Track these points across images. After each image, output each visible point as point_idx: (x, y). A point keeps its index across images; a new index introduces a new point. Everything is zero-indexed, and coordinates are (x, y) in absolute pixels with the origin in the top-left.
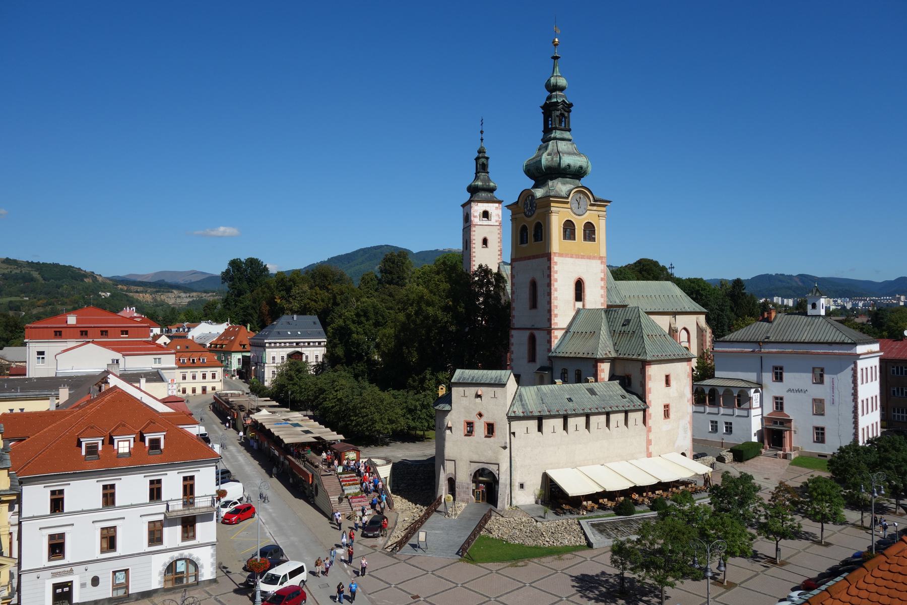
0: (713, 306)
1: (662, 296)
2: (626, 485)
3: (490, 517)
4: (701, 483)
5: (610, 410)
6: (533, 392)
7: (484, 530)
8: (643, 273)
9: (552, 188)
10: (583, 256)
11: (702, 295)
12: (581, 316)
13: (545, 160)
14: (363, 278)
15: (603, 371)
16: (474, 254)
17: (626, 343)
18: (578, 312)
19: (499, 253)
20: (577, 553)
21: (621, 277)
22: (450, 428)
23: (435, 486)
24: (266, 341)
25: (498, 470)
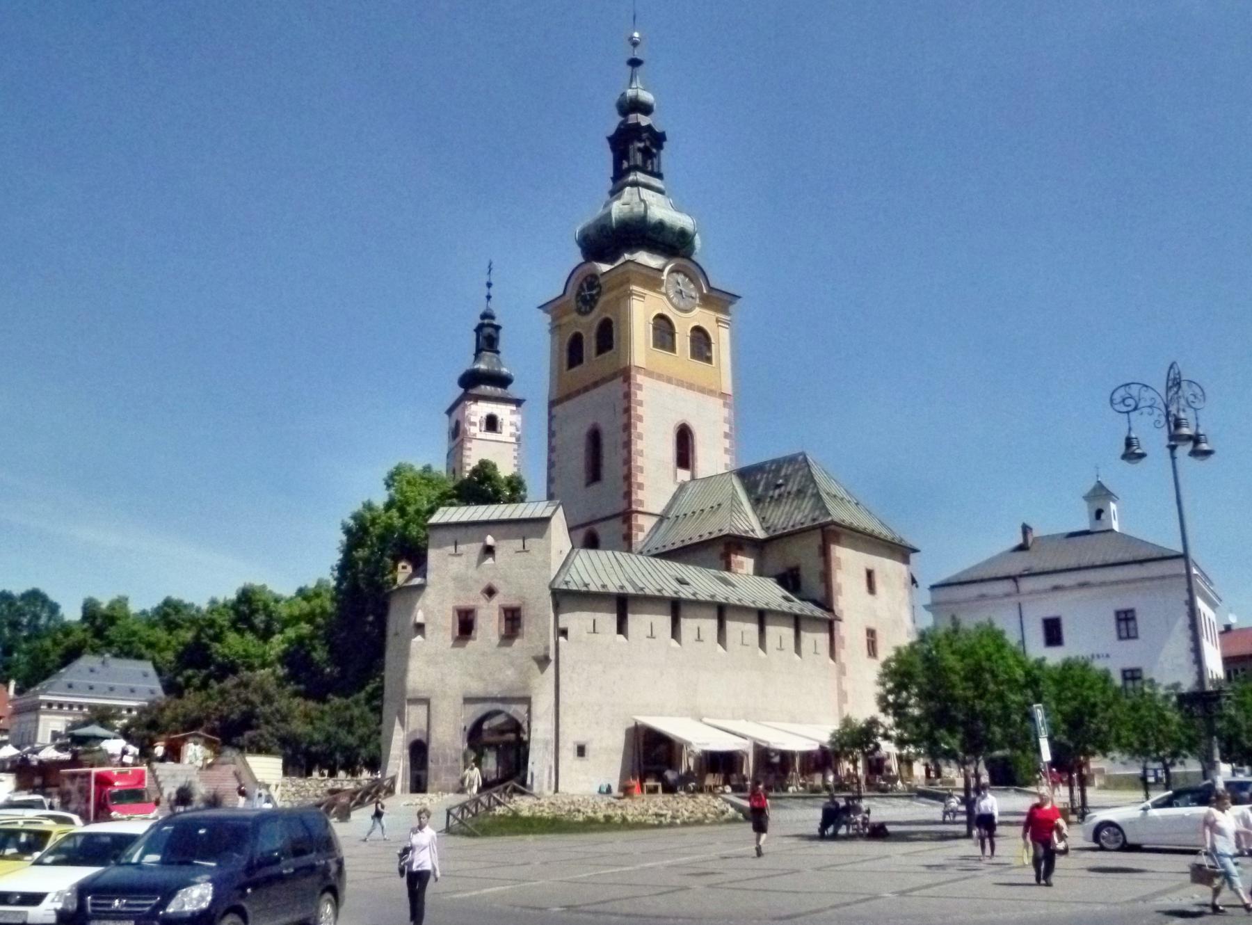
18: (682, 487)
24: (42, 697)
25: (529, 711)
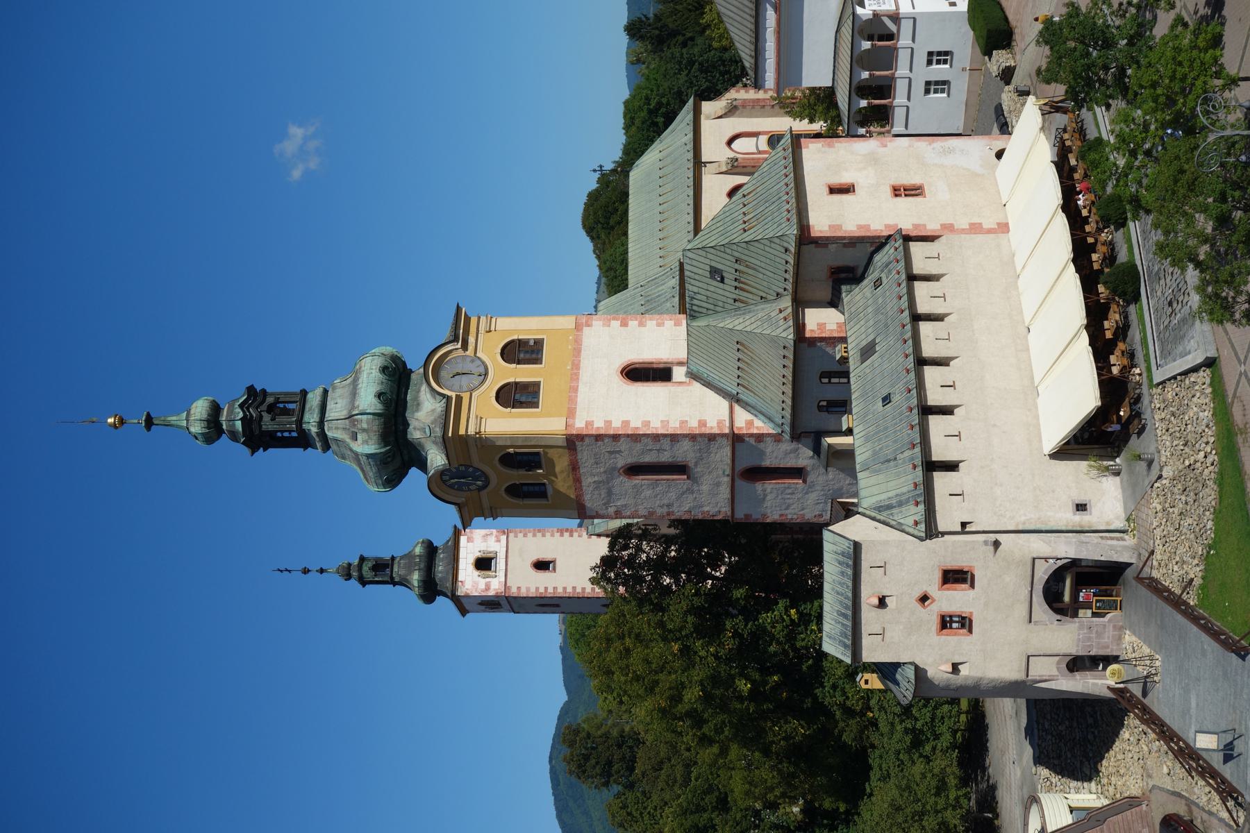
0: (681, 82)
1: (660, 191)
2: (1072, 281)
3: (1151, 579)
4: (1061, 119)
5: (907, 313)
6: (873, 480)
7: (1185, 596)
8: (612, 222)
9: (427, 430)
10: (573, 364)
11: (660, 104)
12: (704, 371)
13: (367, 445)
14: (621, 825)
15: (821, 326)
16: (569, 590)
17: (761, 276)
18: (693, 376)
19: (566, 534)
20: (1230, 394)
21: (620, 269)
22: (955, 668)
23: (1085, 700)
25: (1046, 559)
